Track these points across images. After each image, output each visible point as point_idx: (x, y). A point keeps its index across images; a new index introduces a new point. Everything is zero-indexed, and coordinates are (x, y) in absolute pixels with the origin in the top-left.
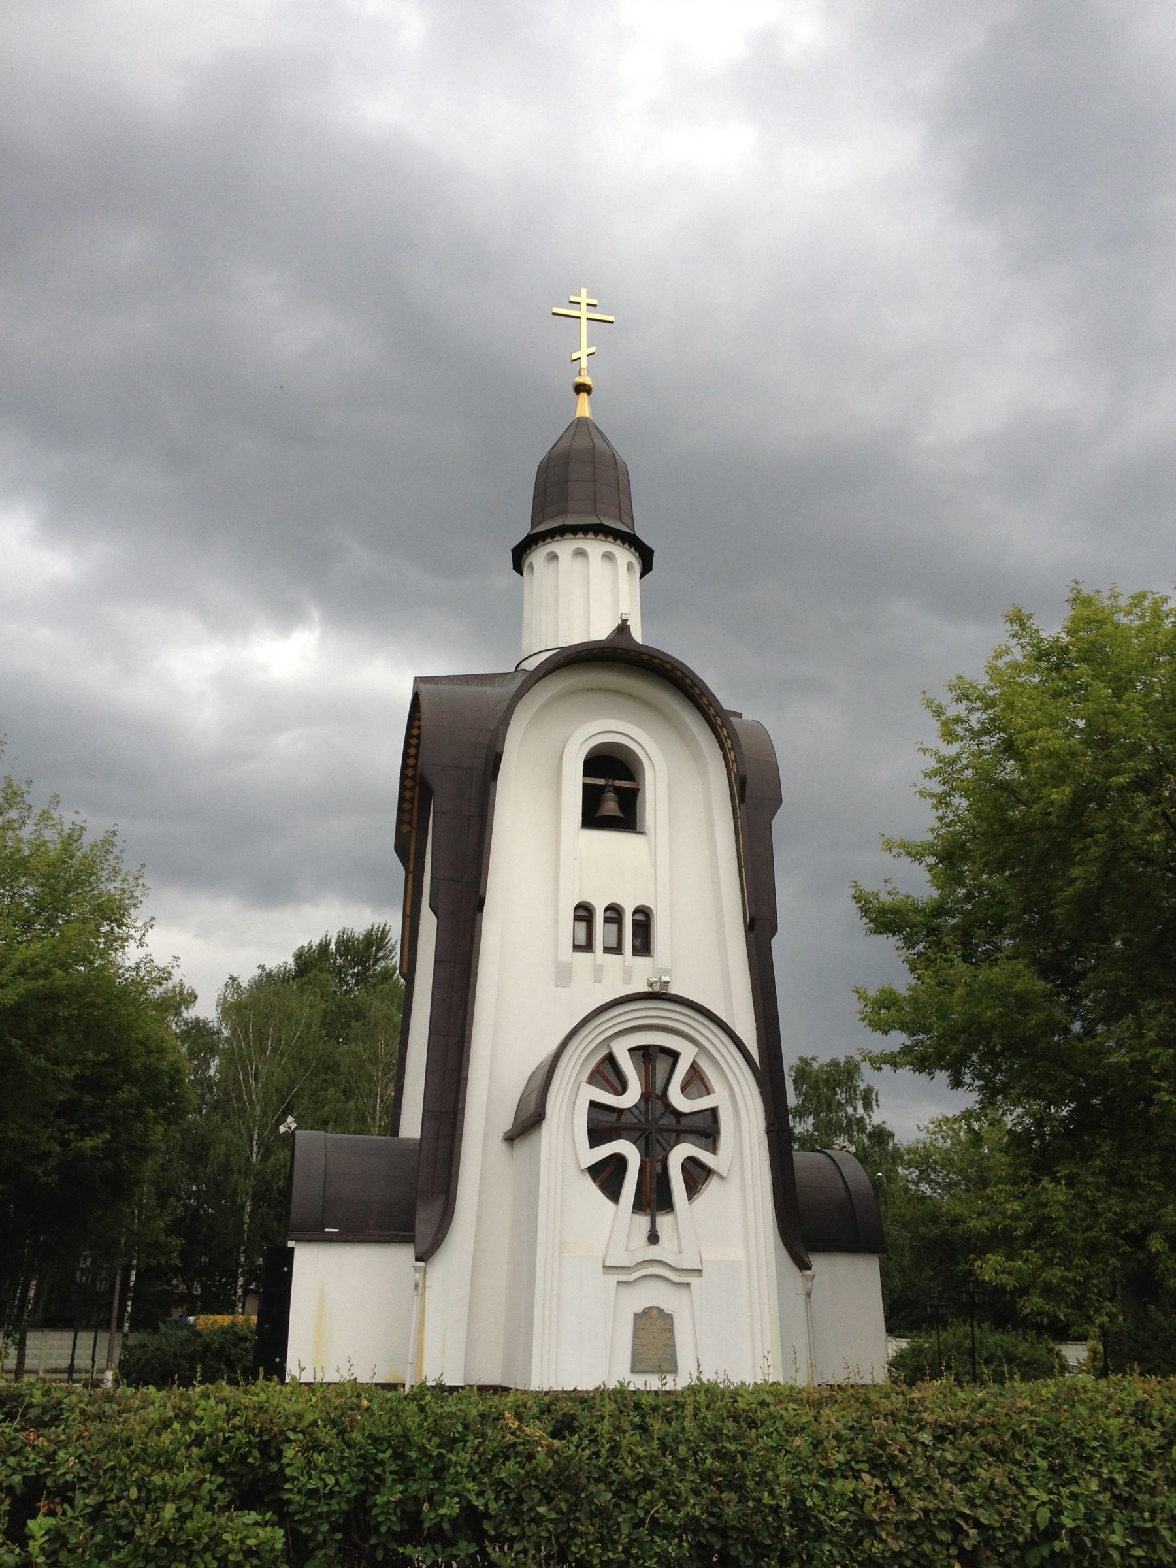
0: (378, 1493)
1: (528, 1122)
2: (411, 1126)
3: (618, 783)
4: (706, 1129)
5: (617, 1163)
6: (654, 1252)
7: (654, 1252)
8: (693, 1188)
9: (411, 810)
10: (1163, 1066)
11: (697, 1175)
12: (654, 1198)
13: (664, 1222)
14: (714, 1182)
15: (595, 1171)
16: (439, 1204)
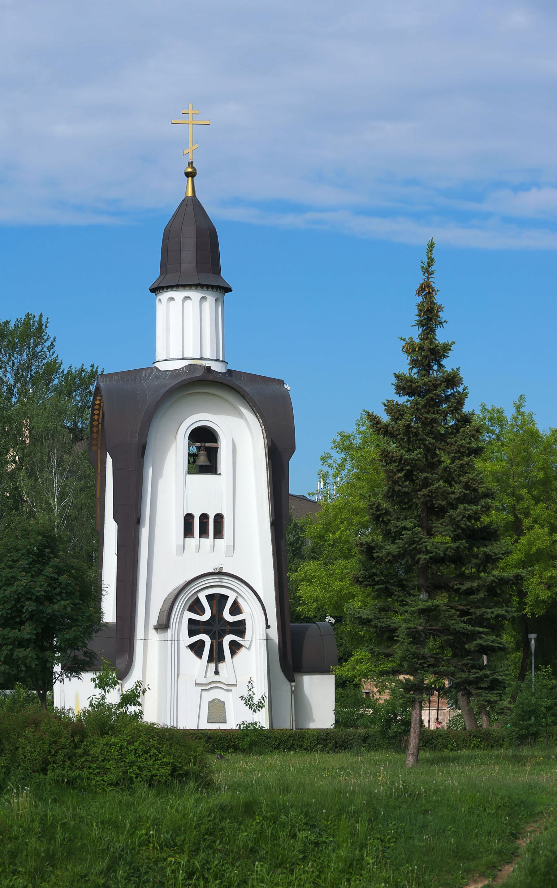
0: (418, 372)
1: (163, 626)
2: (109, 612)
3: (208, 445)
4: (239, 628)
5: (202, 643)
6: (217, 678)
7: (217, 678)
8: (233, 653)
9: (97, 438)
10: (431, 597)
11: (235, 647)
12: (217, 656)
13: (221, 666)
14: (243, 650)
15: (192, 647)
16: (127, 655)
